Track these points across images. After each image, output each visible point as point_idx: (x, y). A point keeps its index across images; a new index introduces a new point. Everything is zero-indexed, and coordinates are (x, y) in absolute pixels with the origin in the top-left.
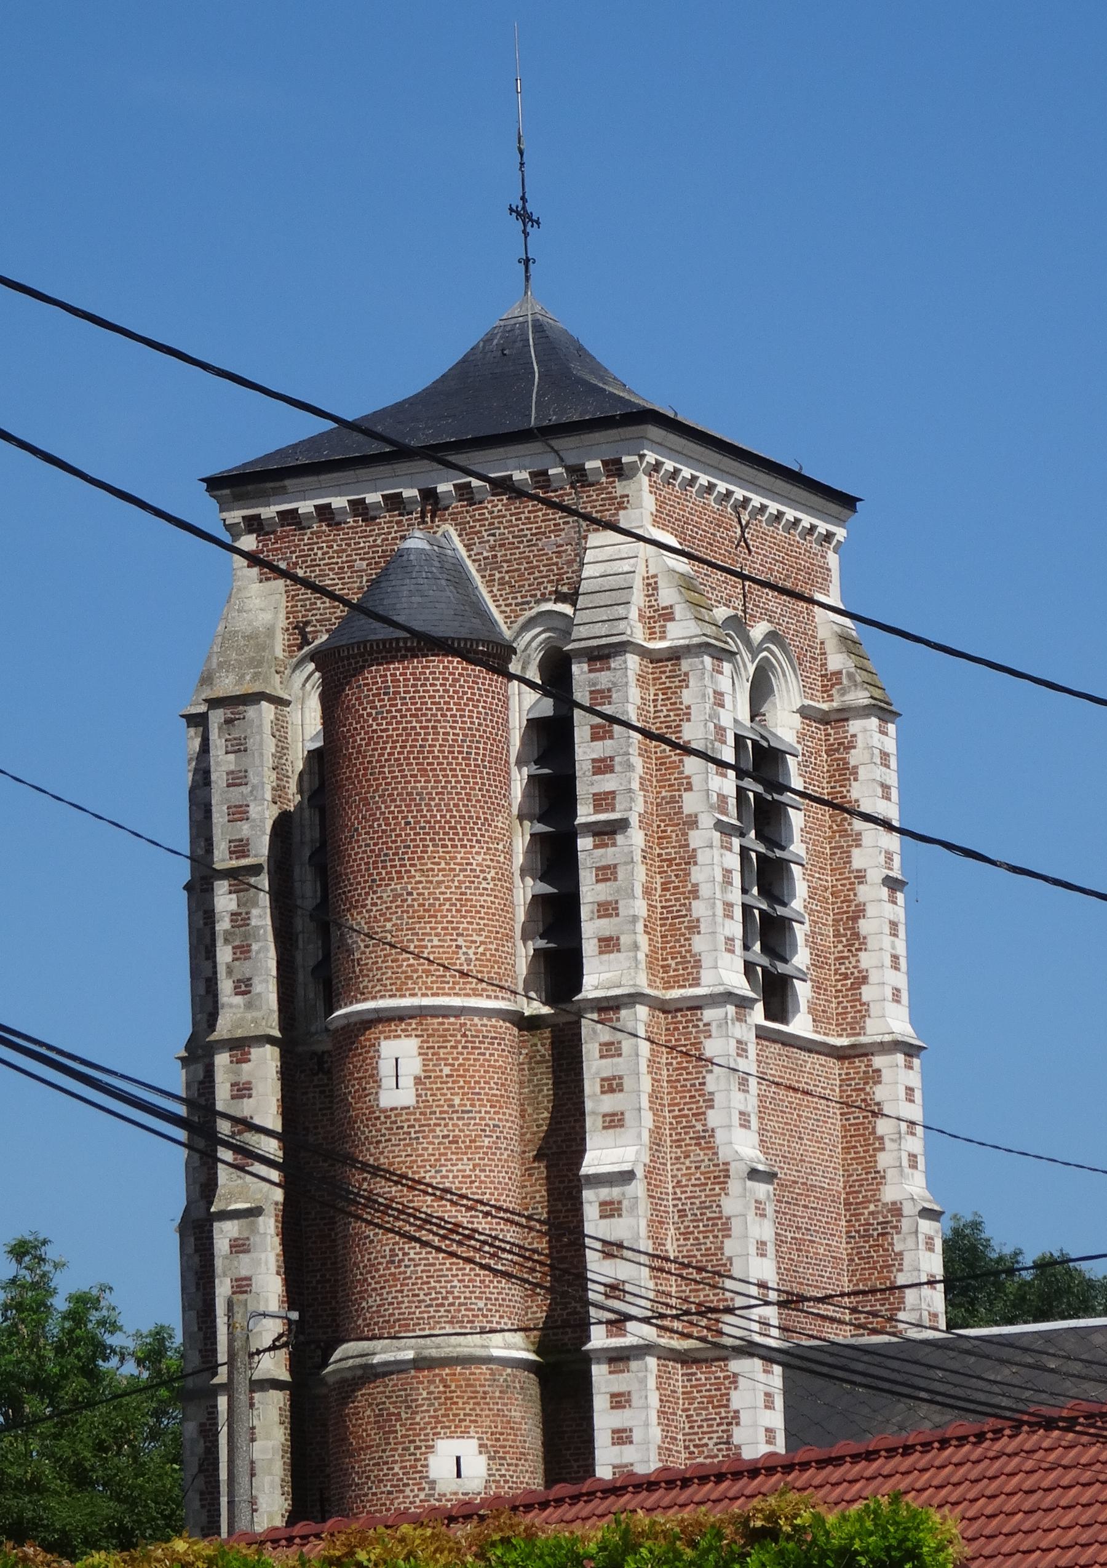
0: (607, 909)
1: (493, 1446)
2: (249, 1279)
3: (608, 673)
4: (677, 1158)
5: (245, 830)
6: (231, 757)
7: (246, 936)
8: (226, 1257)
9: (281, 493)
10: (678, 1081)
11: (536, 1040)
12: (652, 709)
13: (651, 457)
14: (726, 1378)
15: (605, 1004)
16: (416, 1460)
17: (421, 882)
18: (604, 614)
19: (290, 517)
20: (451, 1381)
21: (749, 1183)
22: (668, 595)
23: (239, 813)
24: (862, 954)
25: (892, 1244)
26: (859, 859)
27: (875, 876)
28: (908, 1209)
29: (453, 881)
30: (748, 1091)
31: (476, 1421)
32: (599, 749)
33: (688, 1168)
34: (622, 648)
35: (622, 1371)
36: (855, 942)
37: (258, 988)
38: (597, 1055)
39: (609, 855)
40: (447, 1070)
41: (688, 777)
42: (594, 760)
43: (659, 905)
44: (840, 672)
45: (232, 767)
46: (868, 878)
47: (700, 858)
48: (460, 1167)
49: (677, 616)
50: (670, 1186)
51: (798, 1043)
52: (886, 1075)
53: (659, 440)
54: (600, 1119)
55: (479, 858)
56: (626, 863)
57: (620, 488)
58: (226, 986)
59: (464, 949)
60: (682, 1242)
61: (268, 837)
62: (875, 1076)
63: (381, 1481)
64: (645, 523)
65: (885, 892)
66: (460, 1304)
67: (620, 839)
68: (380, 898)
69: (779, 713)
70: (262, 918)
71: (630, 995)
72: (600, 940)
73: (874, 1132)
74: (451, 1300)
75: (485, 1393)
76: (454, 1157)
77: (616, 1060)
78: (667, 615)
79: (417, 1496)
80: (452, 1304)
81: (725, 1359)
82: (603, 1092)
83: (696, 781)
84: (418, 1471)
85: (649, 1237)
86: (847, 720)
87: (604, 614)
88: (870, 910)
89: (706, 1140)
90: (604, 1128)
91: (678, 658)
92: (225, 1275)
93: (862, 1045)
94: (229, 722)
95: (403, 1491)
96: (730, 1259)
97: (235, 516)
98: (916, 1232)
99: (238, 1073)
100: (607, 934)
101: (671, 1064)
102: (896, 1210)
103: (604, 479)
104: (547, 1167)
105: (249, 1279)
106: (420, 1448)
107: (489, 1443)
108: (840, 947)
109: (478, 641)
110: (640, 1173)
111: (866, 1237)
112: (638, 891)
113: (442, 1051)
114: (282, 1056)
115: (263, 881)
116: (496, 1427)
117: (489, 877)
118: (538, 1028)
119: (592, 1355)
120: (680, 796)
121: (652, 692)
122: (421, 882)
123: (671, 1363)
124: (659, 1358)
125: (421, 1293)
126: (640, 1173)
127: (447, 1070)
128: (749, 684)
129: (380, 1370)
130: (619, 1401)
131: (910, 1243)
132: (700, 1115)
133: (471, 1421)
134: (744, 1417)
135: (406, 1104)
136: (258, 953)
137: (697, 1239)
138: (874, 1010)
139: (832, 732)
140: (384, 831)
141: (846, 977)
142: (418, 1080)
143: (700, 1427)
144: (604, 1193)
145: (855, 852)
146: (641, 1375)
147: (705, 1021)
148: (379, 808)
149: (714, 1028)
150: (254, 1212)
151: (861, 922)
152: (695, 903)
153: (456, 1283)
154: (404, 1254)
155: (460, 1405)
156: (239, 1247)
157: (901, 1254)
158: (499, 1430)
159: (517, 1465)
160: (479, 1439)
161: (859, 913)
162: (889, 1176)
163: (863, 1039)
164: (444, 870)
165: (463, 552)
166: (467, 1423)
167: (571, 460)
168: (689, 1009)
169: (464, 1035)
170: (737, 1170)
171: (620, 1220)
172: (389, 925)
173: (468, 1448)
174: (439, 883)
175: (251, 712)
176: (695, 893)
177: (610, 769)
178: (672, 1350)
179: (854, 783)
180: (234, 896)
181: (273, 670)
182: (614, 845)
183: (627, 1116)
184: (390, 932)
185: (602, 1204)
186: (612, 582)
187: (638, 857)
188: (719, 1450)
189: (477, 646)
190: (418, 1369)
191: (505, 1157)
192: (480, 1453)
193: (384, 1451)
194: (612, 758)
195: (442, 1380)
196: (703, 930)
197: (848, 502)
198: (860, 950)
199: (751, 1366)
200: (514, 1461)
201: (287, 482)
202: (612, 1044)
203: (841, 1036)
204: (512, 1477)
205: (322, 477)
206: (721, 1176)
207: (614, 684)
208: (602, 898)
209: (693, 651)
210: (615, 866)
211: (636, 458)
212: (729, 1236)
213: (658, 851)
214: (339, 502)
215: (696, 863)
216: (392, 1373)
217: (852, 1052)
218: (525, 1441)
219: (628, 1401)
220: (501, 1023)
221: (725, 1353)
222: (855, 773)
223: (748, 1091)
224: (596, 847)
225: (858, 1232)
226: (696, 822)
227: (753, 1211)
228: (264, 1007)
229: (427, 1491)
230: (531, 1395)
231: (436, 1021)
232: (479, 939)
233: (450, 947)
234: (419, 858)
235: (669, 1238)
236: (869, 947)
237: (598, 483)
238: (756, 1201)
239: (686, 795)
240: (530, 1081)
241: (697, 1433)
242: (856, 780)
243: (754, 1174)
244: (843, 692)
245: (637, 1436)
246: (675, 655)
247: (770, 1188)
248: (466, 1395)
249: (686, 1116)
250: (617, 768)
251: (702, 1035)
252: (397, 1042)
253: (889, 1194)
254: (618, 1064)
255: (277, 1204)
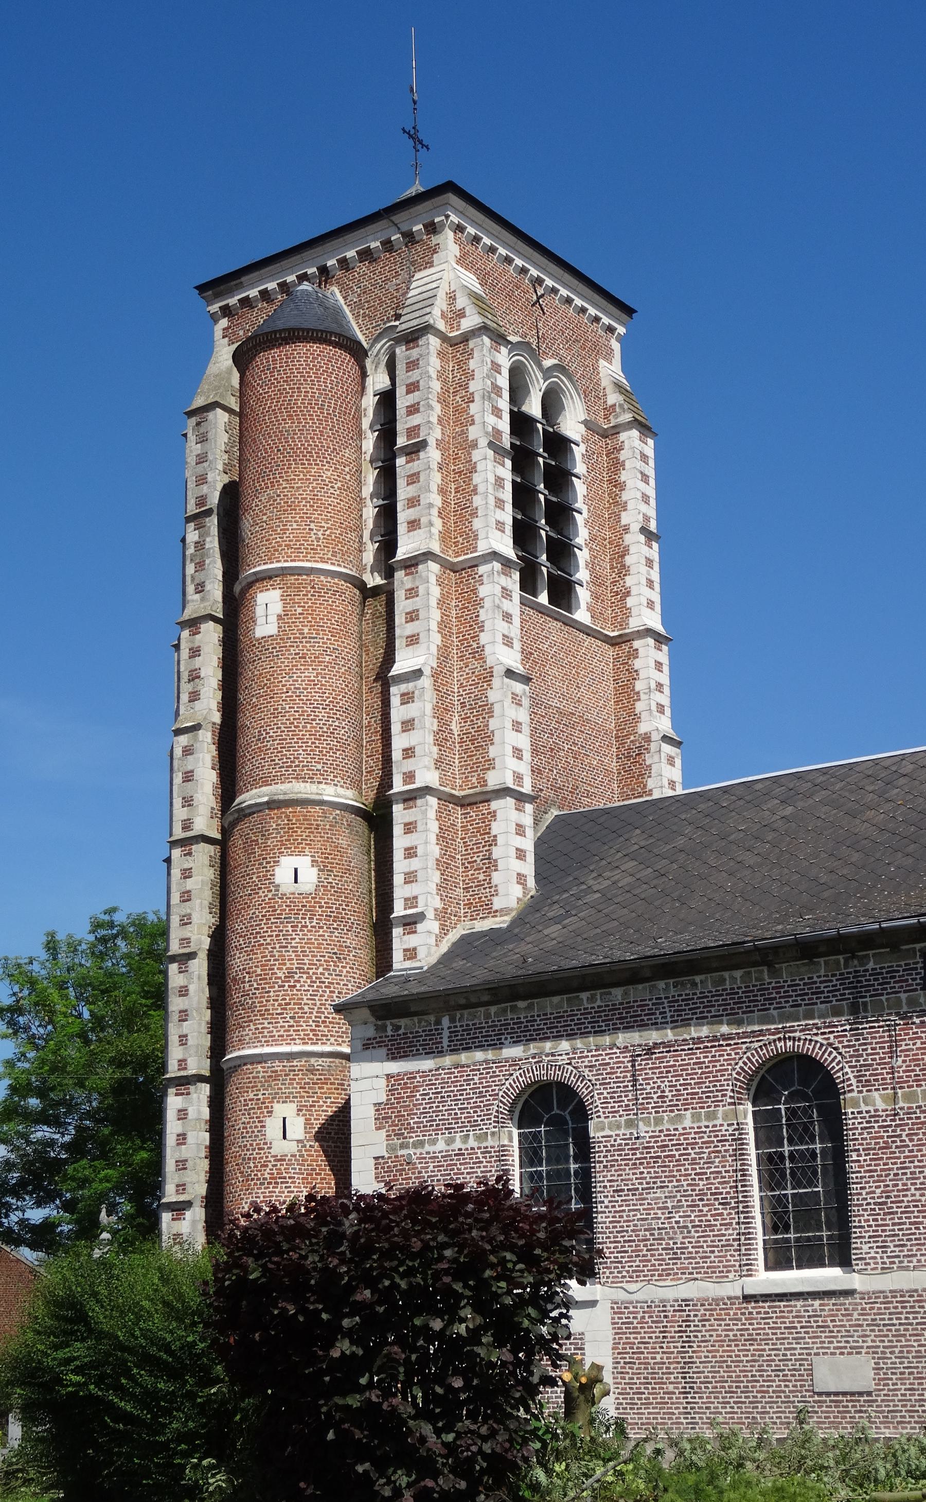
0: (413, 502)
1: (322, 862)
2: (192, 771)
3: (417, 349)
4: (461, 668)
5: (205, 489)
6: (199, 445)
7: (202, 556)
8: (180, 759)
9: (240, 287)
10: (462, 616)
11: (376, 603)
12: (451, 377)
13: (454, 219)
14: (489, 813)
15: (409, 563)
16: (267, 871)
17: (286, 488)
18: (417, 314)
19: (246, 302)
20: (293, 816)
21: (506, 680)
22: (462, 302)
23: (202, 480)
24: (627, 578)
25: (644, 760)
26: (625, 519)
27: (635, 527)
28: (655, 737)
29: (308, 487)
30: (511, 623)
31: (310, 844)
32: (411, 399)
33: (467, 674)
34: (426, 329)
35: (412, 807)
36: (623, 570)
37: (208, 587)
38: (404, 598)
39: (415, 466)
40: (299, 610)
41: (472, 416)
42: (407, 407)
43: (453, 503)
44: (615, 405)
45: (199, 452)
46: (631, 529)
47: (479, 468)
48: (306, 674)
49: (467, 314)
50: (456, 687)
51: (577, 626)
52: (641, 652)
53: (461, 209)
54: (405, 640)
55: (329, 474)
56: (425, 470)
57: (435, 240)
58: (190, 588)
59: (315, 531)
60: (463, 724)
61: (218, 493)
62: (635, 654)
63: (245, 887)
64: (449, 259)
65: (642, 538)
66: (303, 766)
67: (422, 455)
68: (260, 501)
69: (568, 422)
70: (213, 543)
71: (424, 554)
72: (408, 523)
73: (633, 690)
74: (297, 763)
75: (317, 825)
76: (303, 668)
77: (416, 599)
78: (461, 314)
79: (266, 896)
80: (298, 766)
81: (488, 801)
82: (407, 622)
83: (477, 418)
84: (268, 877)
85: (434, 717)
86: (618, 433)
87: (417, 314)
88: (632, 550)
89: (479, 653)
90: (407, 646)
91: (467, 340)
92: (179, 771)
93: (626, 634)
94: (198, 424)
95: (258, 893)
96: (493, 732)
97: (215, 308)
98: (660, 750)
99: (193, 642)
100: (413, 518)
101: (458, 606)
102: (647, 738)
103: (425, 237)
104: (381, 685)
105: (192, 771)
106: (270, 862)
107: (320, 860)
108: (614, 575)
109: (331, 333)
110: (427, 671)
111: (629, 757)
112: (434, 488)
113: (296, 597)
114: (224, 632)
115: (214, 519)
116: (326, 849)
117: (336, 486)
118: (379, 595)
119: (393, 799)
120: (467, 430)
121: (451, 365)
122: (286, 488)
123: (451, 805)
124: (439, 799)
125: (277, 759)
126: (427, 671)
127: (299, 610)
128: (541, 394)
129: (247, 811)
130: (410, 828)
131: (656, 758)
132: (475, 637)
133: (306, 844)
134: (500, 840)
135: (271, 634)
136: (209, 565)
137: (472, 721)
138: (634, 612)
139: (608, 441)
140: (264, 457)
141: (617, 593)
142: (279, 617)
143: (472, 849)
144: (404, 687)
145: (623, 514)
146: (423, 808)
147: (480, 574)
148: (261, 443)
149: (485, 578)
150: (196, 728)
151: (627, 557)
152: (475, 498)
153: (301, 752)
154: (267, 733)
155: (299, 833)
156: (188, 751)
157: (650, 766)
158: (328, 851)
159: (342, 877)
160: (312, 856)
161: (625, 552)
162: (642, 717)
163: (627, 631)
164: (302, 479)
165: (342, 301)
166: (304, 845)
167: (404, 228)
168: (469, 568)
169: (313, 587)
170: (499, 671)
171: (413, 704)
172: (265, 518)
173: (304, 863)
174: (298, 488)
175: (211, 415)
176: (475, 491)
177: (417, 411)
178: (452, 796)
179: (622, 472)
180: (197, 532)
181: (229, 393)
182: (418, 459)
183: (421, 636)
184: (265, 522)
185: (402, 695)
186: (425, 296)
187: (435, 466)
188: (484, 864)
189: (331, 336)
190: (270, 809)
191: (343, 670)
192: (313, 866)
193: (247, 867)
194: (418, 403)
195: (287, 816)
196: (479, 514)
197: (629, 311)
198: (625, 575)
199: (504, 807)
200: (340, 874)
201: (243, 279)
202: (413, 589)
203: (613, 631)
204: (337, 884)
205: (262, 271)
206: (487, 676)
207: (421, 355)
208: (409, 496)
209: (477, 333)
210: (419, 473)
211: (443, 218)
212: (493, 716)
213: (453, 467)
214: (272, 285)
215: (476, 472)
216: (254, 813)
217: (620, 640)
218: (350, 862)
219: (415, 827)
220: (343, 583)
221: (488, 797)
222: (623, 464)
223: (511, 623)
224: (407, 462)
225: (623, 754)
226: (476, 445)
227: (510, 700)
228: (212, 599)
229: (273, 892)
230: (357, 832)
231: (293, 578)
232: (326, 525)
233: (304, 529)
234: (286, 472)
235: (454, 722)
236: (631, 572)
237: (422, 240)
238: (512, 693)
239: (470, 428)
240: (373, 630)
241: (469, 854)
242: (624, 469)
243: (510, 673)
244: (616, 417)
245: (420, 851)
246: (465, 338)
247: (527, 688)
248: (303, 826)
249: (467, 639)
250: (421, 409)
251: (477, 584)
252: (268, 593)
253: (643, 728)
254: (416, 602)
255: (214, 724)
